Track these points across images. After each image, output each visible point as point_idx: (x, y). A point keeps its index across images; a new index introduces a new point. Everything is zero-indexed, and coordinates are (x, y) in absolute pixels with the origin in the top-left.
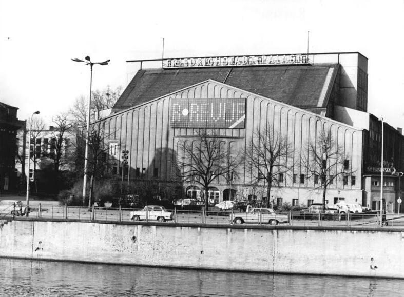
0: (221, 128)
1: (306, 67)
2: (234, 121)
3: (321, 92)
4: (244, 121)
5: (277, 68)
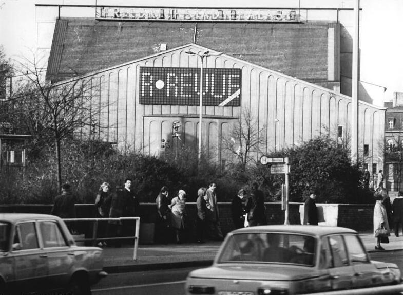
0: (173, 105)
1: (297, 26)
2: (225, 97)
3: (326, 60)
4: (238, 97)
5: (258, 25)
